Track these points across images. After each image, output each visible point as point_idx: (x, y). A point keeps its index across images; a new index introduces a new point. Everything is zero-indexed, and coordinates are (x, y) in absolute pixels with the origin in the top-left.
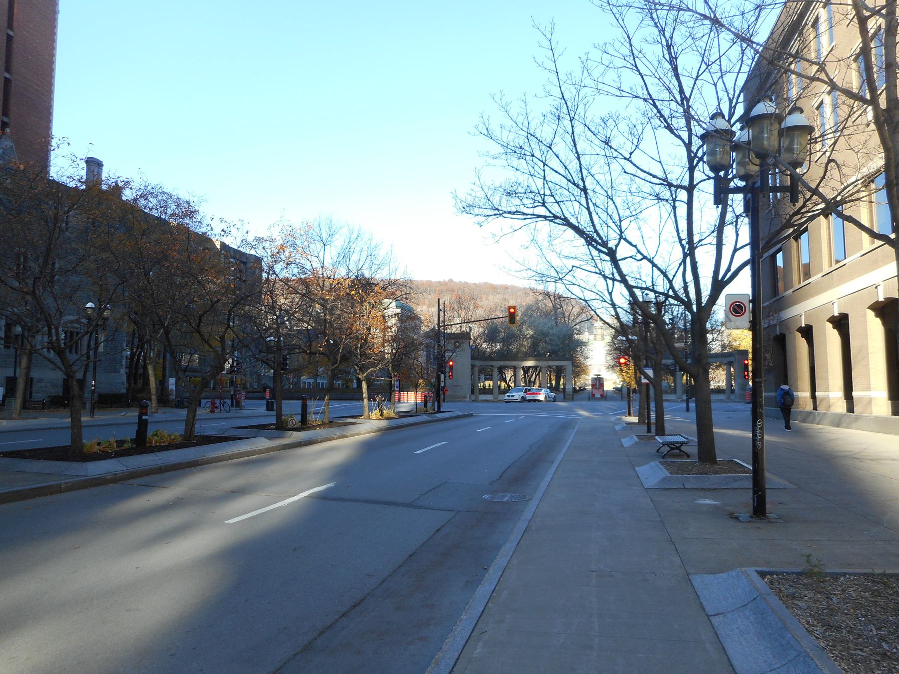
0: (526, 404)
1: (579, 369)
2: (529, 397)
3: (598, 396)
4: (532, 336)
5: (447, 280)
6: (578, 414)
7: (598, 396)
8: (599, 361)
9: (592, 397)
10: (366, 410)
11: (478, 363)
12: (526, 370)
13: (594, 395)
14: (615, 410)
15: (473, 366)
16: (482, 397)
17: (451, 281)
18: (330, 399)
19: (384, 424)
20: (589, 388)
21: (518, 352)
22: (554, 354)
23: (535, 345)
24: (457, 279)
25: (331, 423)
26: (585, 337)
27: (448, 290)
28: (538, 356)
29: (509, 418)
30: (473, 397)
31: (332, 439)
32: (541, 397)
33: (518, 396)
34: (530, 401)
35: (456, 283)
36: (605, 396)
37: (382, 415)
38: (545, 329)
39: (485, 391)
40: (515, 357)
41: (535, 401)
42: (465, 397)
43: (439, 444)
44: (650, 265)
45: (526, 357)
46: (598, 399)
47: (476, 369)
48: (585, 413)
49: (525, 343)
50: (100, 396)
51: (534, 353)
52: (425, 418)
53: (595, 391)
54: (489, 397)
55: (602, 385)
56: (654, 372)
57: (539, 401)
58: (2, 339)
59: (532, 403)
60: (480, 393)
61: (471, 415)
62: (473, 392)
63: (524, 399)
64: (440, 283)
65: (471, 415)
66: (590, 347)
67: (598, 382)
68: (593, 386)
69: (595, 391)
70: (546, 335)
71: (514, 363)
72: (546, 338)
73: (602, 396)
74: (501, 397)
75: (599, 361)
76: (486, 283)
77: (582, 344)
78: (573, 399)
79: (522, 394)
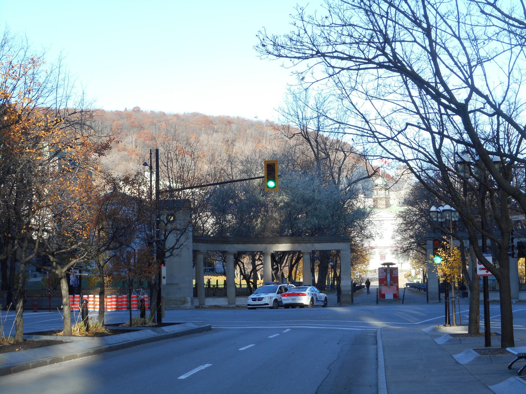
0: (282, 311)
1: (358, 255)
2: (286, 300)
3: (389, 296)
4: (287, 205)
5: (130, 108)
6: (367, 324)
7: (389, 296)
8: (384, 242)
9: (380, 297)
10: (68, 321)
11: (203, 247)
12: (278, 259)
13: (383, 296)
14: (422, 318)
15: (195, 252)
16: (210, 301)
17: (137, 110)
18: (25, 308)
19: (94, 343)
20: (375, 284)
21: (264, 229)
22: (318, 233)
23: (290, 220)
24: (146, 107)
25: (26, 343)
26: (361, 202)
27: (133, 126)
28: (296, 236)
29: (286, 329)
30: (197, 303)
31: (44, 364)
32: (305, 300)
33: (268, 298)
34: (287, 306)
35: (145, 115)
36: (399, 298)
37: (87, 330)
38: (308, 193)
39: (214, 292)
40: (260, 238)
41: (294, 306)
42: (185, 302)
43: (202, 367)
44: (438, 10)
45: (277, 239)
46: (390, 302)
47: (201, 257)
48: (378, 324)
49: (276, 215)
50: (70, 294)
51: (291, 229)
52: (148, 333)
53: (384, 290)
54: (221, 301)
55: (395, 279)
56: (476, 150)
57: (302, 306)
58: (523, 287)
59: (290, 309)
60: (208, 295)
61: (208, 329)
62: (196, 295)
63: (278, 304)
64: (118, 114)
65: (208, 329)
66: (373, 217)
67: (389, 274)
68: (382, 281)
69: (384, 290)
70: (307, 202)
71: (260, 247)
72: (300, 205)
73: (395, 296)
74: (241, 301)
75: (384, 242)
76: (195, 115)
77: (362, 214)
78: (351, 303)
79: (274, 296)
